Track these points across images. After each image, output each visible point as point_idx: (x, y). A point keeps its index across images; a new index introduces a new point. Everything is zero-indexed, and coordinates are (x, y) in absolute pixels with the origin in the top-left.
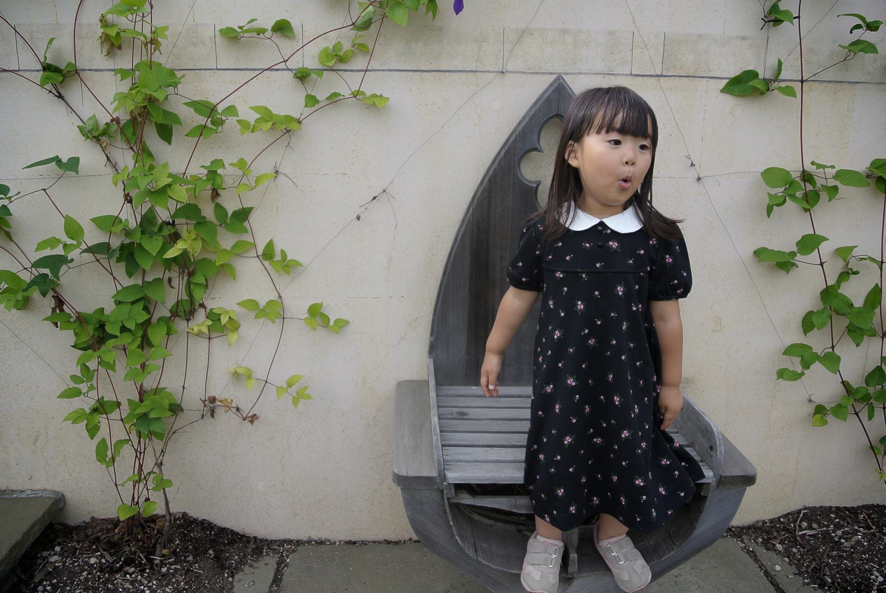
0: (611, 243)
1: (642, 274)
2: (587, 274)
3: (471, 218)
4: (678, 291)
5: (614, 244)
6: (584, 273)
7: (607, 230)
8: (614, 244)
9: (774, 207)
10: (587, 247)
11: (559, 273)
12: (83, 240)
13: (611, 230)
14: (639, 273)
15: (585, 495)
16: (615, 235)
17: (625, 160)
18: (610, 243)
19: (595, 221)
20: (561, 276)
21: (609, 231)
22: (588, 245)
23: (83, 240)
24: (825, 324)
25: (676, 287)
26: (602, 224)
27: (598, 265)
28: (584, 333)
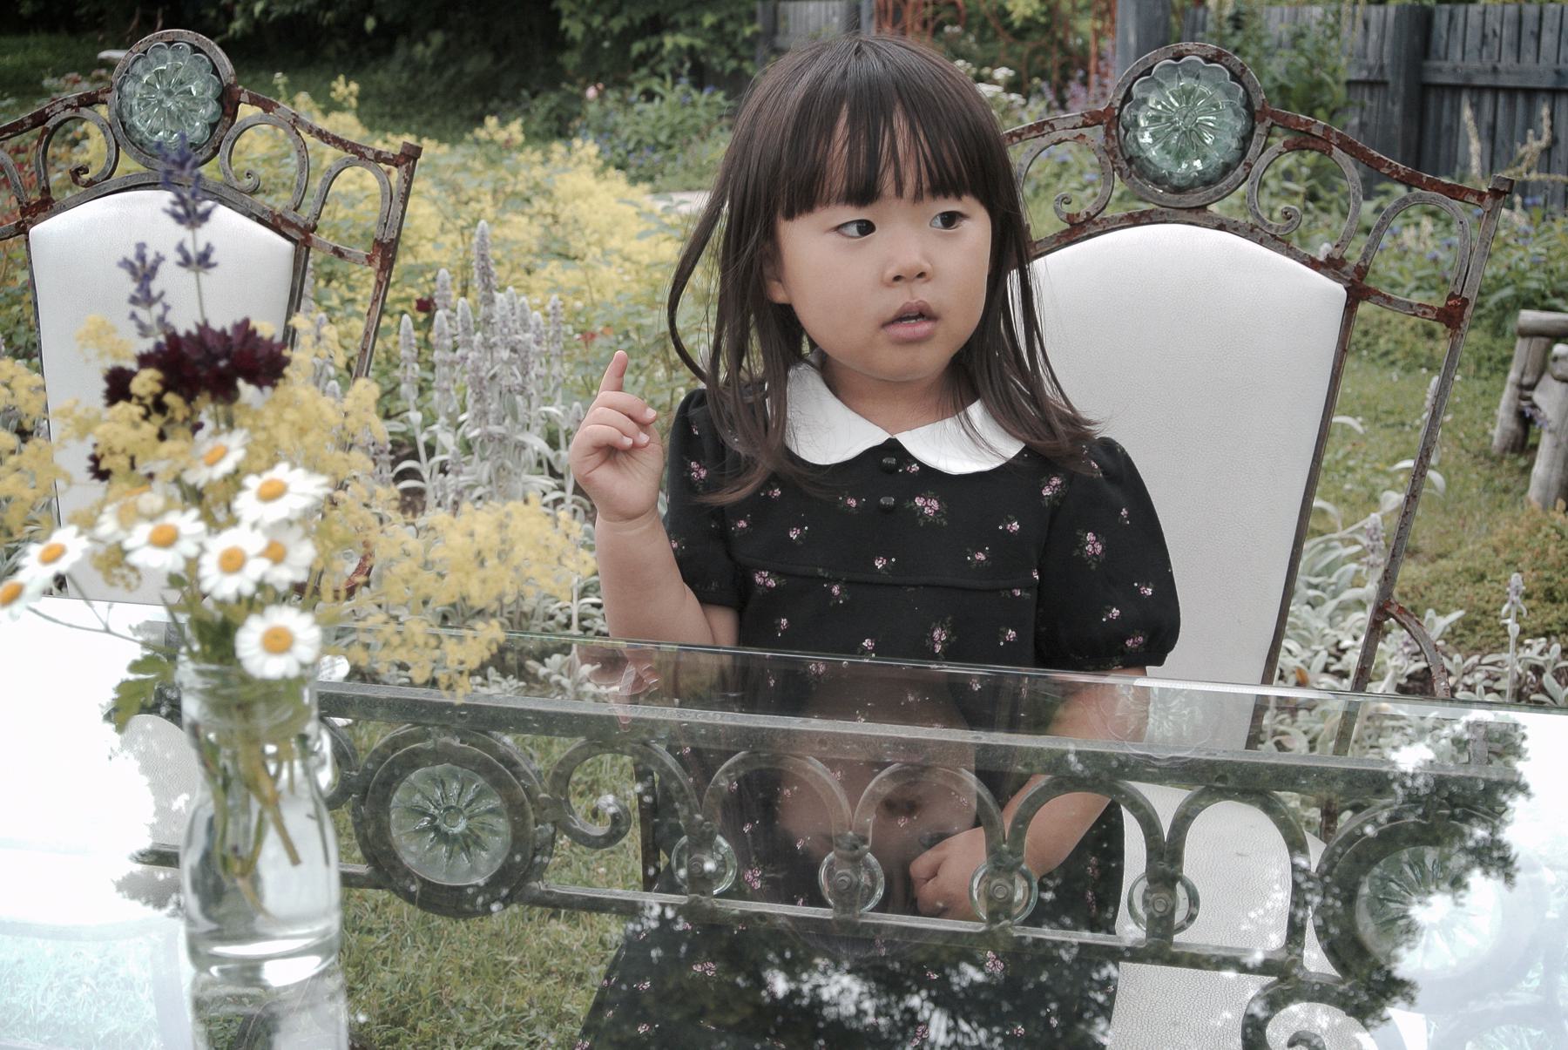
0: (919, 502)
1: (1018, 593)
2: (848, 584)
3: (785, 149)
4: (1129, 643)
5: (928, 506)
6: (837, 581)
7: (910, 464)
8: (928, 506)
9: (290, 323)
10: (850, 506)
11: (766, 574)
12: (1558, 61)
13: (920, 464)
14: (1010, 590)
15: (780, 985)
16: (932, 478)
17: (891, 272)
18: (279, 75)
19: (874, 436)
20: (772, 583)
21: (915, 468)
22: (853, 503)
23: (1558, 61)
24: (333, 195)
25: (1118, 635)
26: (893, 447)
27: (879, 564)
28: (782, 632)
